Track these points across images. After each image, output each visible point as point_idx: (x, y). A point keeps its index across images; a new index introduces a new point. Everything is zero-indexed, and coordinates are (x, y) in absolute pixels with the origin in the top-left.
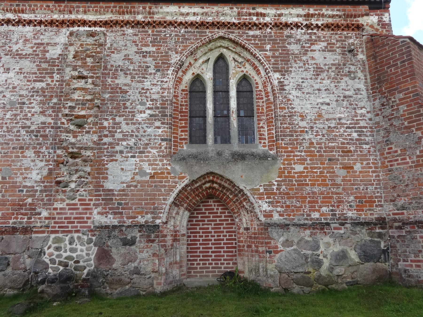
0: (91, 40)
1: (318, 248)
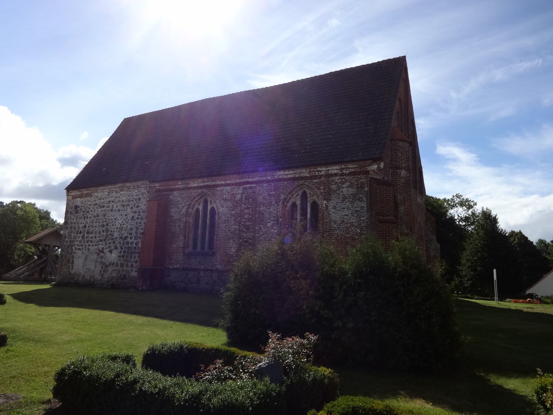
0: (250, 191)
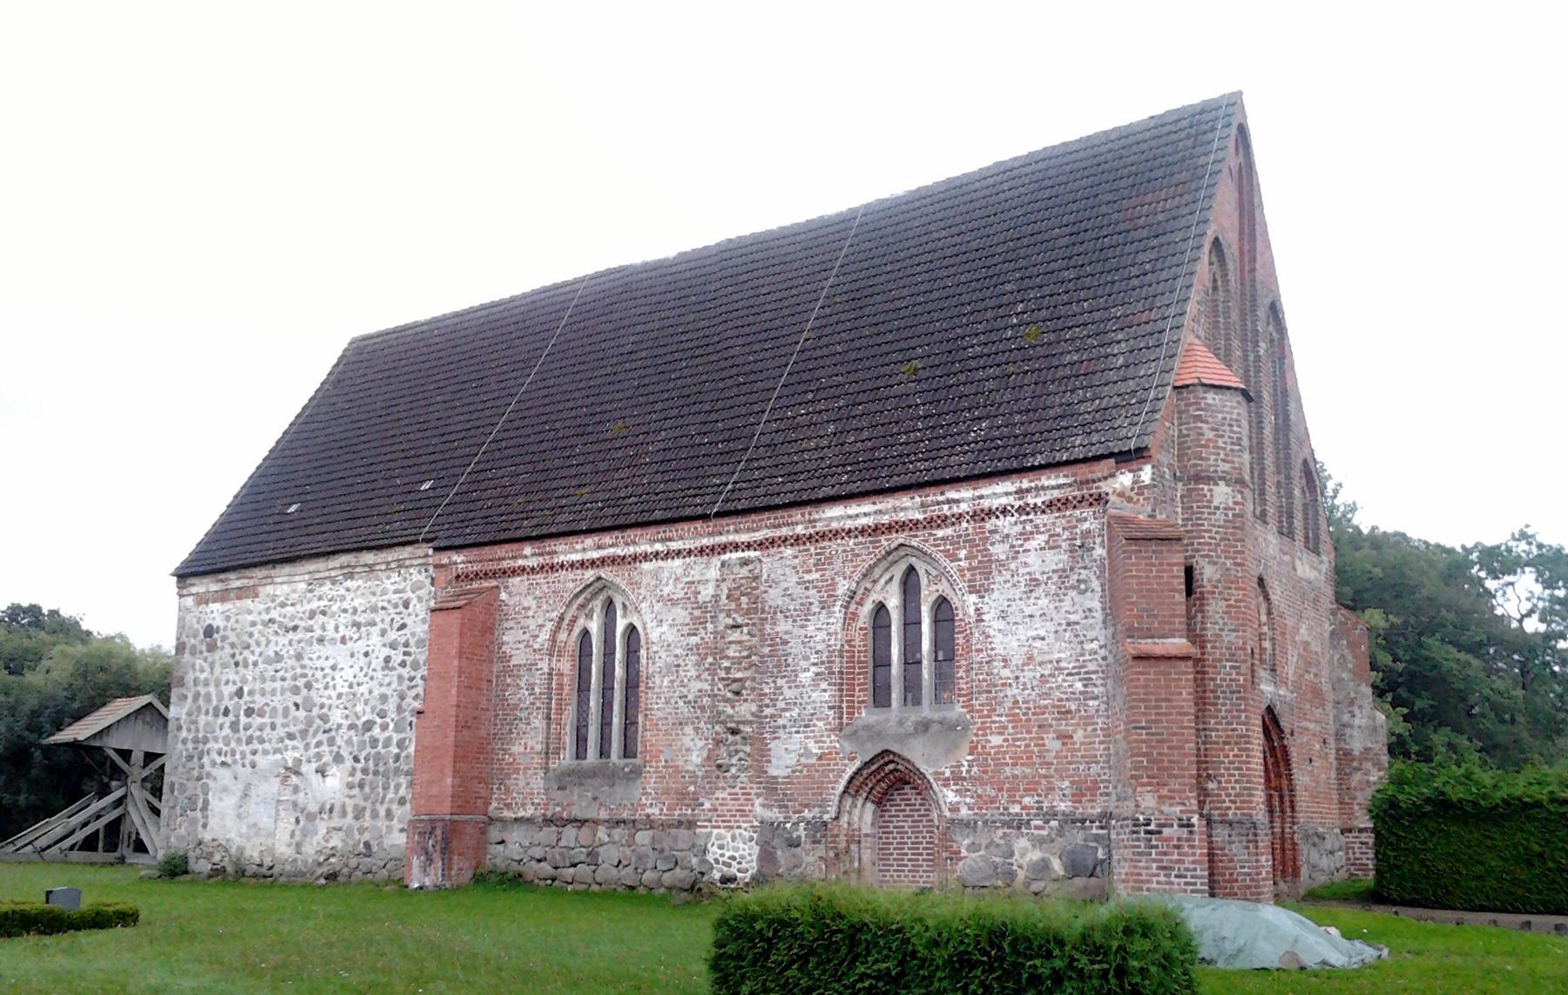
0: (744, 571)
1: (1012, 854)
